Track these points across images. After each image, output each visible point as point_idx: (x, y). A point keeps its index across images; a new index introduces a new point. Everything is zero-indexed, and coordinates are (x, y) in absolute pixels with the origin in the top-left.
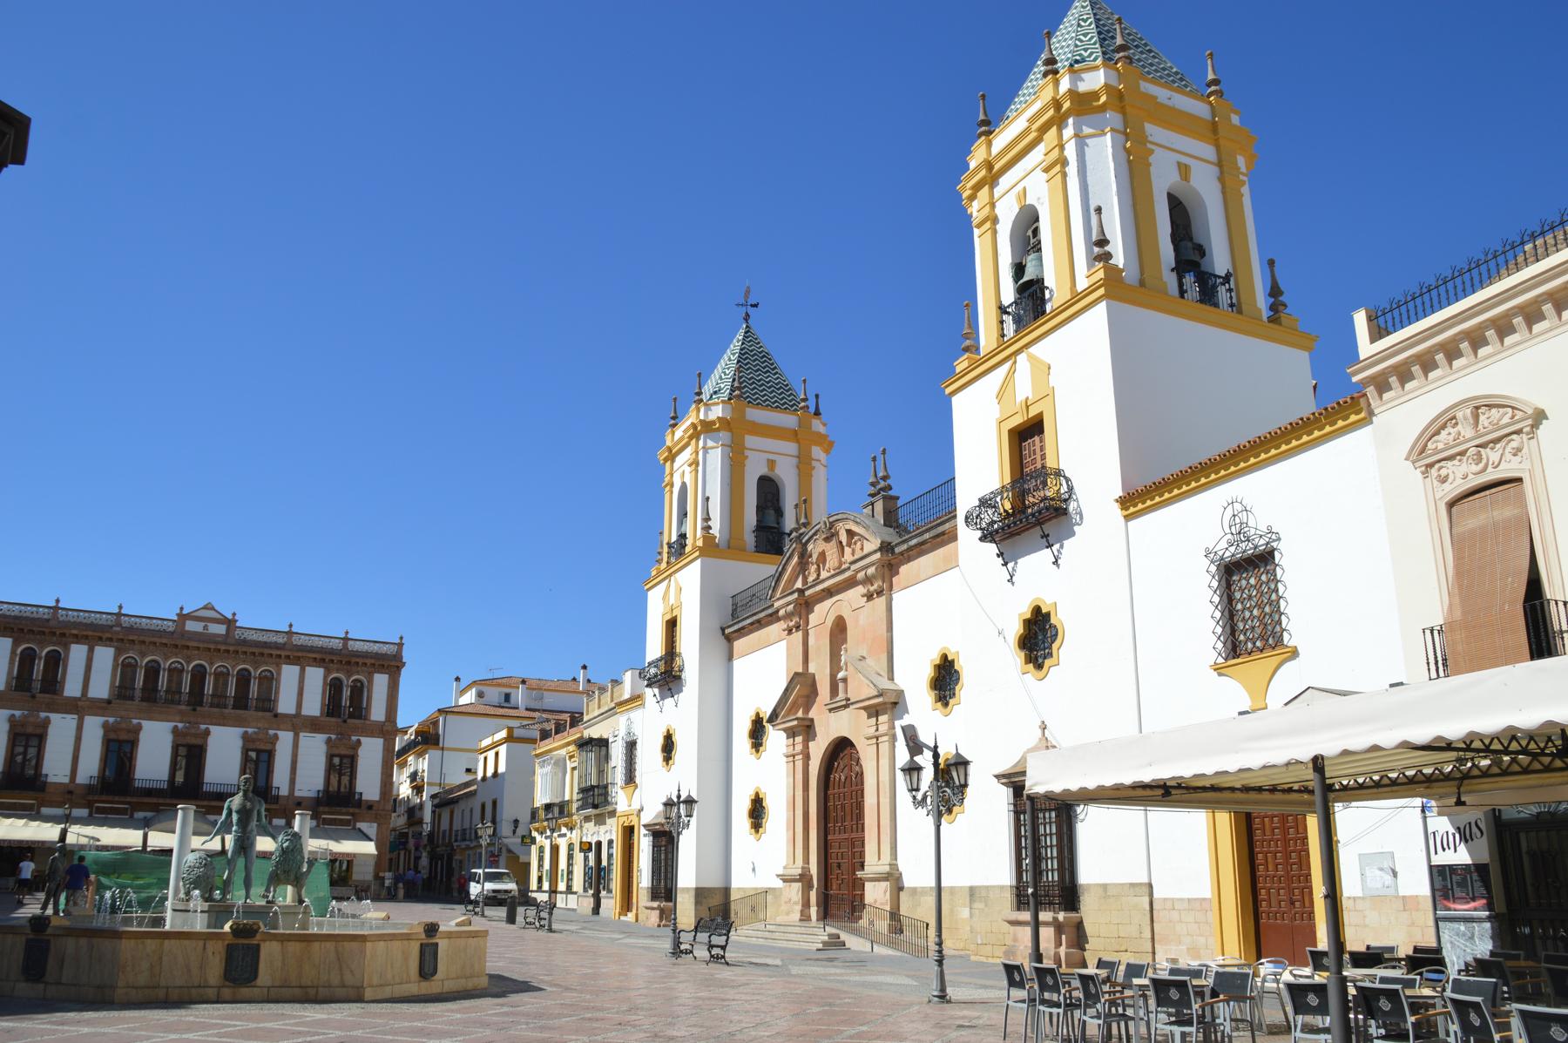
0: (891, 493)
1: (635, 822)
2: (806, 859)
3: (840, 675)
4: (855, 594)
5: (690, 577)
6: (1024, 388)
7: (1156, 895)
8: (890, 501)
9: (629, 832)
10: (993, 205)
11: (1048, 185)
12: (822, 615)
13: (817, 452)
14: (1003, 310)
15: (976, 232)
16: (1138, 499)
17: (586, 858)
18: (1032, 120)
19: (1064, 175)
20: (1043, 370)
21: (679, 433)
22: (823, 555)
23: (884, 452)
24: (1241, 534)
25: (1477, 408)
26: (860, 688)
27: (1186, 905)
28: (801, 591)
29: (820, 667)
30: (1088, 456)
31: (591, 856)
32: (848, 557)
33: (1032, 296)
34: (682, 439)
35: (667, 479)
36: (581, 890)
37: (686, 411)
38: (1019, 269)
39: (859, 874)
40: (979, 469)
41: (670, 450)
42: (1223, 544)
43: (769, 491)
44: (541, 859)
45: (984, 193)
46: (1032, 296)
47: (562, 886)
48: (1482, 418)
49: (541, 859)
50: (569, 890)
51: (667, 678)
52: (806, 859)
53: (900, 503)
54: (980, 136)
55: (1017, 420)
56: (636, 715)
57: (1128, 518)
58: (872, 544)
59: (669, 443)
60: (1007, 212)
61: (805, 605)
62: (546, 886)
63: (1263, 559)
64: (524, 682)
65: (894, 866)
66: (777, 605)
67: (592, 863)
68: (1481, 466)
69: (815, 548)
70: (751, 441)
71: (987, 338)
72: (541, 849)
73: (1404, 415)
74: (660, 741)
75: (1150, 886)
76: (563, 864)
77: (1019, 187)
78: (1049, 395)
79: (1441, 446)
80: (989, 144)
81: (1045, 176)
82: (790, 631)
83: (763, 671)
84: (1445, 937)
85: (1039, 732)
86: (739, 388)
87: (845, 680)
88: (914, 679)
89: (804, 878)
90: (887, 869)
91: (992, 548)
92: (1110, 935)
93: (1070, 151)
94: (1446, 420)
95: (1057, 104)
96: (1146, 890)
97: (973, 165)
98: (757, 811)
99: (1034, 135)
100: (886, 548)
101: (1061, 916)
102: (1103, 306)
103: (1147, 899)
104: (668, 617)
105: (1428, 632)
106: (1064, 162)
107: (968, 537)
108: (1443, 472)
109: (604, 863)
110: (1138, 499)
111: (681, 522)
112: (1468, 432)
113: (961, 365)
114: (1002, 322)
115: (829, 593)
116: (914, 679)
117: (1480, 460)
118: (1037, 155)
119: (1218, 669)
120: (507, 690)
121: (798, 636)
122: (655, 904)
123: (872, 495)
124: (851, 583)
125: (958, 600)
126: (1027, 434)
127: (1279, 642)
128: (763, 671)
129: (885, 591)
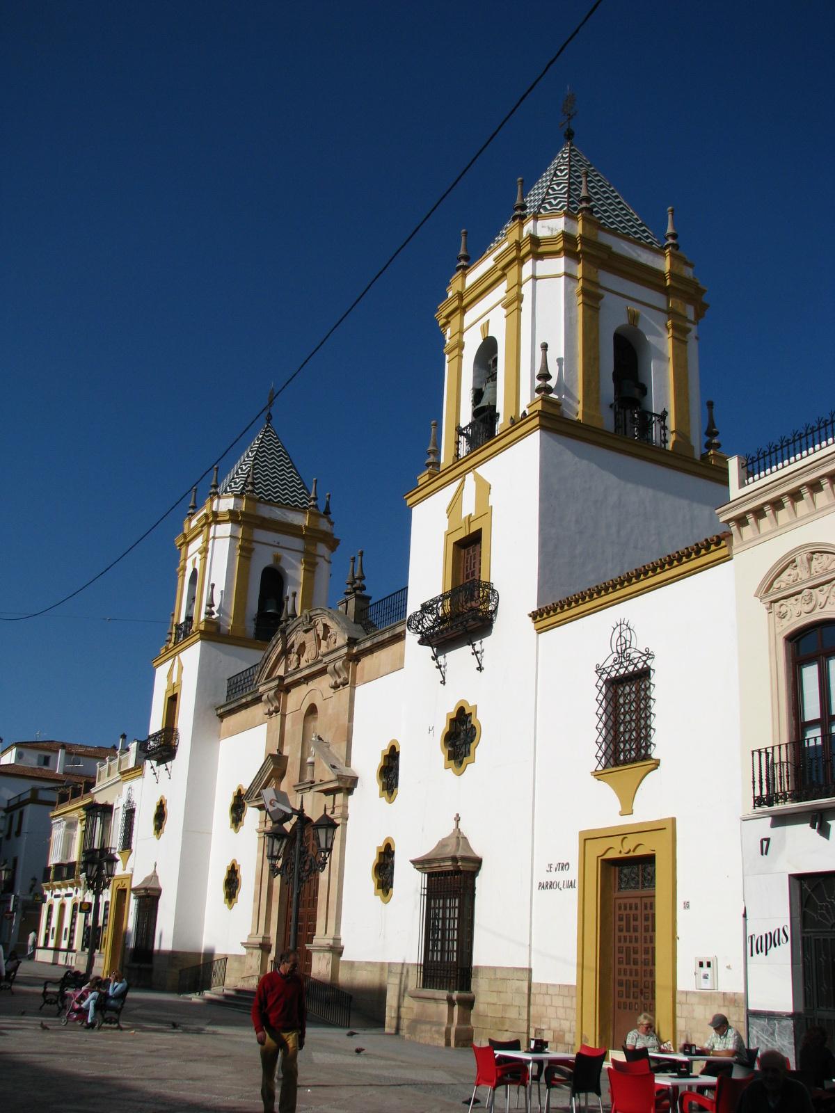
0: (365, 593)
1: (127, 887)
2: (267, 929)
3: (309, 760)
4: (326, 682)
5: (191, 656)
6: (469, 507)
7: (534, 980)
8: (363, 600)
9: (121, 894)
10: (461, 332)
11: (522, 316)
12: (297, 699)
13: (322, 549)
14: (460, 431)
15: (447, 357)
16: (547, 614)
17: (86, 918)
18: (497, 260)
19: (519, 309)
20: (484, 489)
21: (194, 523)
22: (303, 646)
23: (362, 554)
24: (622, 656)
25: (813, 553)
26: (324, 773)
27: (556, 991)
28: (281, 678)
29: (292, 751)
30: (514, 571)
31: (91, 916)
32: (323, 649)
33: (485, 415)
34: (196, 527)
35: (182, 564)
36: (80, 949)
37: (203, 504)
38: (478, 395)
39: (308, 946)
40: (427, 578)
41: (185, 536)
42: (610, 662)
43: (273, 581)
44: (49, 917)
45: (455, 320)
46: (485, 415)
47: (64, 945)
48: (814, 563)
49: (49, 917)
50: (70, 949)
51: (164, 749)
52: (267, 929)
53: (371, 602)
54: (458, 269)
55: (461, 535)
56: (136, 784)
57: (540, 631)
58: (342, 640)
59: (186, 531)
60: (473, 342)
61: (285, 688)
62: (52, 943)
63: (644, 675)
64: (63, 746)
65: (337, 940)
66: (261, 689)
67: (90, 923)
68: (811, 605)
69: (297, 638)
70: (260, 535)
71: (445, 458)
72: (50, 908)
73: (757, 554)
74: (153, 810)
75: (530, 970)
76: (67, 924)
77: (483, 321)
78: (485, 512)
79: (783, 585)
80: (465, 276)
81: (504, 312)
82: (270, 713)
83: (242, 751)
84: (753, 1031)
85: (454, 823)
86: (253, 484)
87: (312, 764)
88: (366, 764)
89: (265, 947)
90: (331, 942)
91: (428, 651)
92: (496, 1011)
93: (526, 290)
94: (788, 563)
95: (518, 245)
96: (526, 975)
97: (450, 294)
98: (232, 883)
99: (499, 273)
100: (352, 642)
101: (455, 995)
102: (539, 431)
103: (526, 984)
104: (170, 694)
105: (756, 754)
106: (519, 298)
107: (412, 638)
108: (783, 609)
109: (100, 924)
110: (547, 614)
111: (190, 607)
112: (804, 575)
113: (423, 478)
114: (458, 443)
115: (307, 679)
116: (366, 764)
117: (811, 600)
118: (500, 292)
119: (596, 774)
120: (47, 754)
121: (277, 718)
122: (136, 965)
123: (347, 593)
124: (323, 672)
125: (400, 697)
126: (468, 548)
127: (647, 757)
128: (242, 751)
129: (346, 683)
